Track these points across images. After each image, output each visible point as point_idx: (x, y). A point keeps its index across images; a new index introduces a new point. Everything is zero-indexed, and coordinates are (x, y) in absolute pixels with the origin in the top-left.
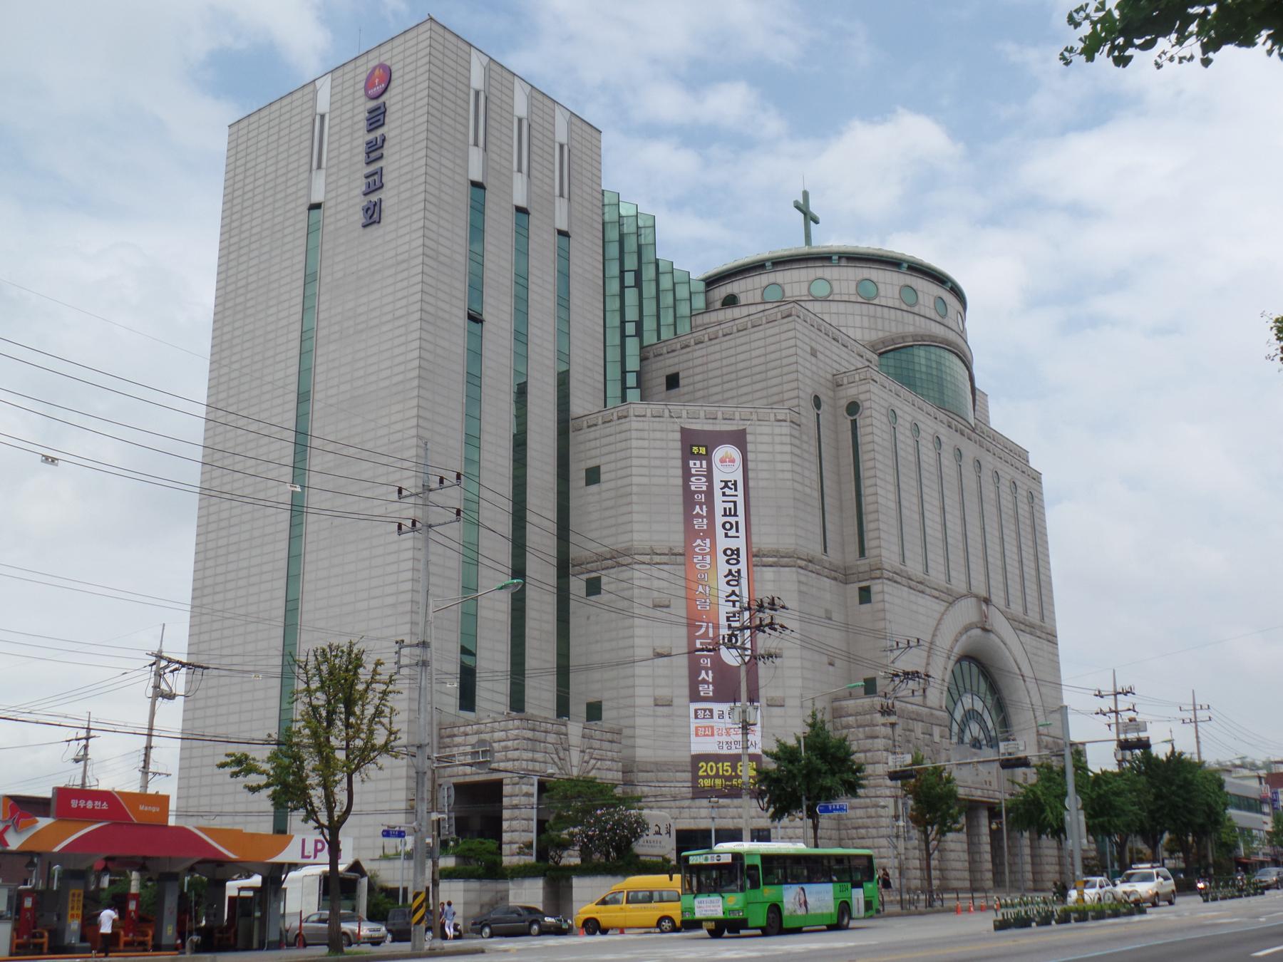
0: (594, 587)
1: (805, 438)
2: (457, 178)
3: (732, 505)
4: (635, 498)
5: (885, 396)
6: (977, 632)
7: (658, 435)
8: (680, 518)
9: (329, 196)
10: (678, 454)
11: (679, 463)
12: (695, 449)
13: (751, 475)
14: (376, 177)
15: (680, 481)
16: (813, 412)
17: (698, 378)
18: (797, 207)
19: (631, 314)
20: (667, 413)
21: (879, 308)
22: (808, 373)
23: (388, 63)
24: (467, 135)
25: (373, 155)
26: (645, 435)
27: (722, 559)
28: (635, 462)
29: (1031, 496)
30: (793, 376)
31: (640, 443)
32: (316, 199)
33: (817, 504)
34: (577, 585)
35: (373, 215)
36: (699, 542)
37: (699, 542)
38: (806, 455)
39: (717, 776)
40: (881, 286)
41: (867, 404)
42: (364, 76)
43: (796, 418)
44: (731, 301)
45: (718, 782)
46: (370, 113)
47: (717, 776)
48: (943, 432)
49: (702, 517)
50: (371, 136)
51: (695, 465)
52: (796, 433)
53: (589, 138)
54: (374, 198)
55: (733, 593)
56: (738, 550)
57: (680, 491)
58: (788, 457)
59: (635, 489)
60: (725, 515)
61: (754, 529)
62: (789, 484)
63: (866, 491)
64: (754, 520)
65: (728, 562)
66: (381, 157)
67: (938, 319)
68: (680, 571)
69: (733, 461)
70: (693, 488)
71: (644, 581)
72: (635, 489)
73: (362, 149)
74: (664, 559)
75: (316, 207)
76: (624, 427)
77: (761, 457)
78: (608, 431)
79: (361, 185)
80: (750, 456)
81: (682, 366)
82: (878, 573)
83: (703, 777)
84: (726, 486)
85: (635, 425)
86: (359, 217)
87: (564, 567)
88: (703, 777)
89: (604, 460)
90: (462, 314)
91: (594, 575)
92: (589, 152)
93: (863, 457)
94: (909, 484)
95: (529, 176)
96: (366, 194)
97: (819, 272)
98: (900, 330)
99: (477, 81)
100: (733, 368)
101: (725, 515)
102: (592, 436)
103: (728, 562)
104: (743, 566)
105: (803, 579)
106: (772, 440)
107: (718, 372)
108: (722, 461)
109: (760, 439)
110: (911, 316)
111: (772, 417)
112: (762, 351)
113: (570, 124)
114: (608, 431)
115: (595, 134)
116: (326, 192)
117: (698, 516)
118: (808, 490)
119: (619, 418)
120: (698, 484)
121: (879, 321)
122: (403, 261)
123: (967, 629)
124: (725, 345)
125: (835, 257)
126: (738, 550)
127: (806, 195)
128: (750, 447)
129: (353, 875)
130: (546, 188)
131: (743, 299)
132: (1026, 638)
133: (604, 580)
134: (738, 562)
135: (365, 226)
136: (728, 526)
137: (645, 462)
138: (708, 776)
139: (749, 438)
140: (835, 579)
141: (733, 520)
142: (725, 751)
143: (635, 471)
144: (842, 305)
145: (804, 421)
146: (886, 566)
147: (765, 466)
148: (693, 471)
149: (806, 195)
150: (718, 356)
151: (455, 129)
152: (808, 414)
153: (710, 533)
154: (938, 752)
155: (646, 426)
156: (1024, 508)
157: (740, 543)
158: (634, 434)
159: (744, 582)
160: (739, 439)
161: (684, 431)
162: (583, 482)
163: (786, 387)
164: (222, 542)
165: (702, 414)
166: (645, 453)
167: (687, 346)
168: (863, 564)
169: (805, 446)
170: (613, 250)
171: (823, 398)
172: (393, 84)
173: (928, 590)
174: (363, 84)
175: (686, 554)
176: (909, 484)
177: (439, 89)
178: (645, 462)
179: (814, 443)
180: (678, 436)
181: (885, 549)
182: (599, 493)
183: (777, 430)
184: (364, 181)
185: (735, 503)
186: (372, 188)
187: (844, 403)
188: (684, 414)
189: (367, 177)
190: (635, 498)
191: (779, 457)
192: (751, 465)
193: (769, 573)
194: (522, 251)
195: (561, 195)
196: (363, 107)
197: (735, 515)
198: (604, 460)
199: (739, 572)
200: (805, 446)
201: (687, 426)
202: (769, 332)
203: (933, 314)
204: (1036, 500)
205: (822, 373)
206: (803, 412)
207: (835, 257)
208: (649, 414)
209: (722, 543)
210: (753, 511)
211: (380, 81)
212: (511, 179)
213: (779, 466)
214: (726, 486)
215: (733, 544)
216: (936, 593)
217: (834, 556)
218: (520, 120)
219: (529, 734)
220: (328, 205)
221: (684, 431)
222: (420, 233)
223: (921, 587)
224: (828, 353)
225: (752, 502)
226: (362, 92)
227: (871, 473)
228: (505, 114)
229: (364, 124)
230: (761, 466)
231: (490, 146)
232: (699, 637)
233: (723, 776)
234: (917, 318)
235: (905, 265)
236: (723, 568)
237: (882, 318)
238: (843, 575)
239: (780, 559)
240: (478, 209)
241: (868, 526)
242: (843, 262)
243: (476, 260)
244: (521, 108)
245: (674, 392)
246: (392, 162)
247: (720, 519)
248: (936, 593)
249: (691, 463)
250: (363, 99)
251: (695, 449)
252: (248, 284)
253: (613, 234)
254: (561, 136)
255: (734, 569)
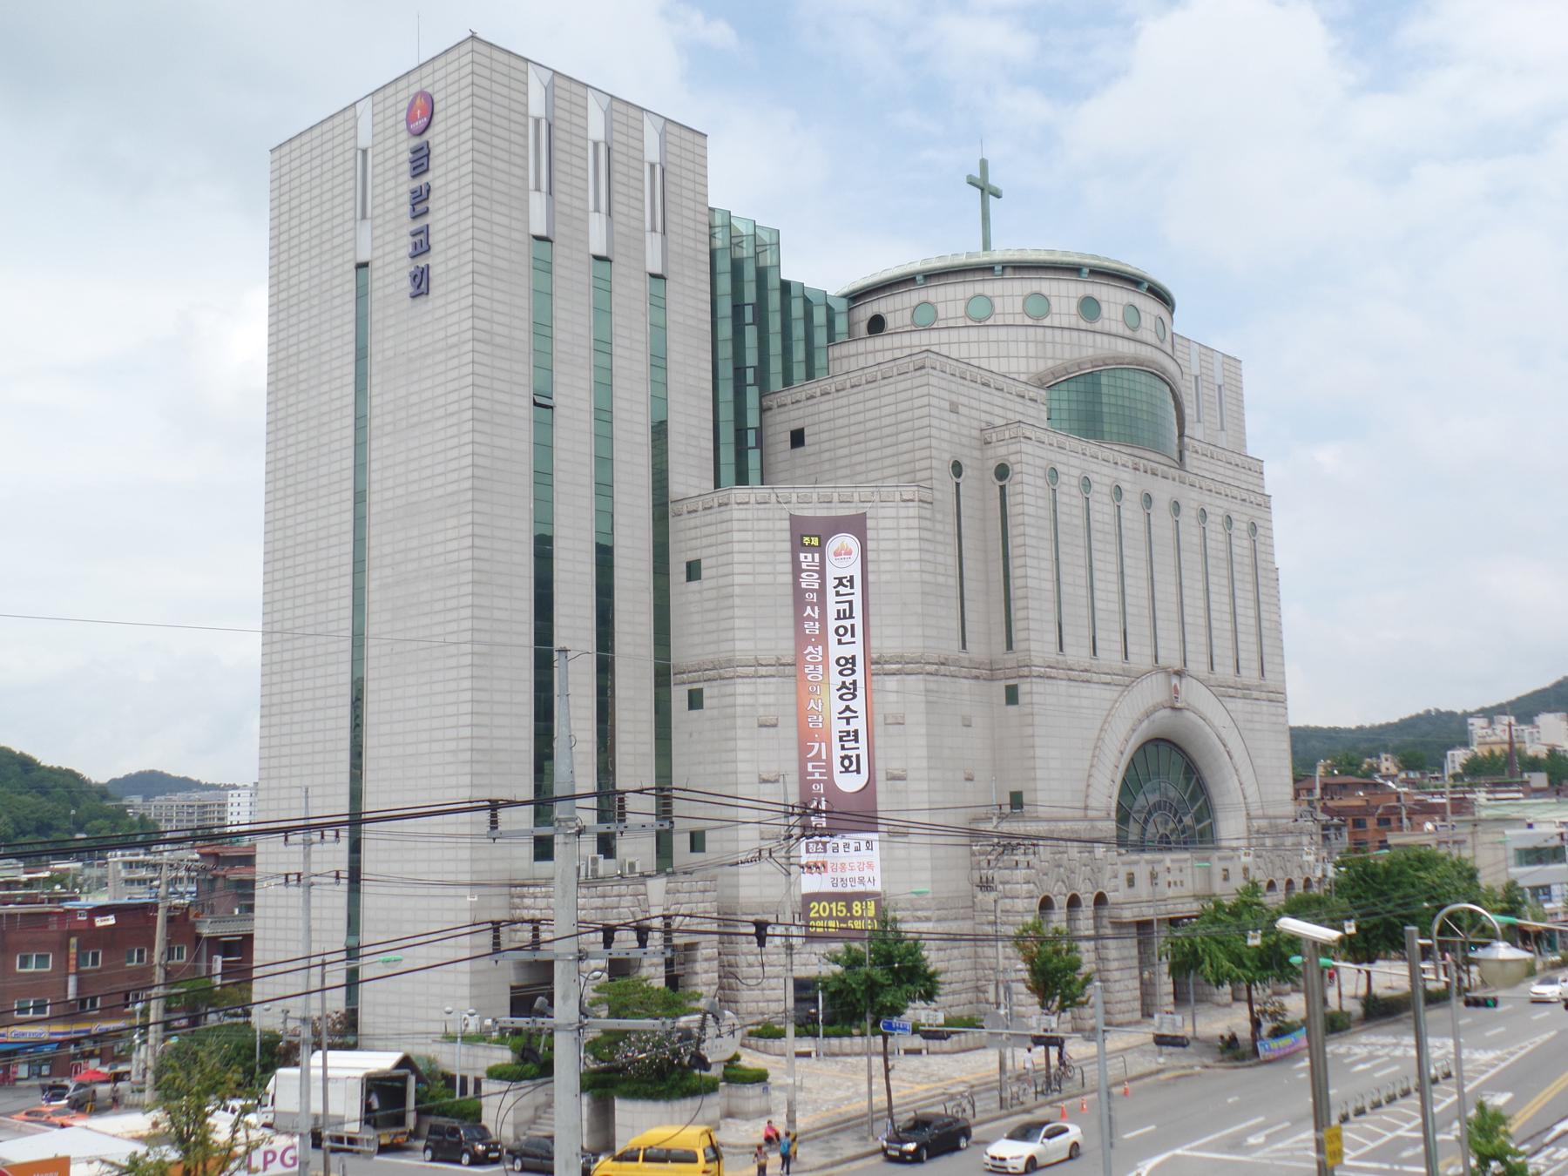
0: (695, 700)
1: (939, 516)
2: (516, 235)
3: (846, 606)
4: (737, 601)
5: (1043, 453)
6: (1167, 712)
7: (763, 525)
8: (791, 622)
9: (379, 252)
10: (788, 546)
11: (788, 557)
12: (806, 540)
13: (871, 567)
14: (422, 237)
15: (789, 579)
16: (951, 482)
17: (824, 436)
18: (972, 182)
19: (751, 358)
20: (773, 498)
21: (1049, 331)
22: (946, 435)
23: (429, 90)
24: (526, 179)
25: (419, 208)
26: (749, 525)
27: (834, 669)
28: (737, 557)
29: (1253, 528)
30: (926, 442)
31: (742, 536)
32: (362, 258)
33: (956, 592)
34: (679, 696)
35: (421, 283)
36: (810, 649)
37: (810, 649)
38: (940, 538)
39: (830, 917)
40: (1053, 301)
41: (1017, 468)
42: (405, 104)
43: (926, 495)
44: (877, 325)
45: (832, 924)
46: (414, 152)
47: (830, 917)
48: (1126, 478)
49: (813, 620)
50: (416, 184)
51: (806, 559)
52: (927, 514)
53: (689, 146)
54: (422, 262)
55: (847, 708)
56: (853, 658)
57: (789, 590)
58: (915, 544)
59: (737, 590)
60: (839, 618)
61: (873, 631)
62: (916, 576)
63: (1015, 572)
64: (873, 621)
65: (841, 673)
66: (426, 212)
67: (1128, 333)
68: (789, 686)
69: (849, 553)
70: (804, 585)
71: (750, 696)
72: (737, 590)
73: (406, 198)
74: (771, 670)
75: (362, 266)
76: (726, 516)
77: (883, 545)
78: (709, 519)
79: (406, 245)
80: (870, 545)
81: (808, 421)
82: (1025, 671)
83: (815, 919)
84: (841, 584)
85: (736, 514)
86: (406, 285)
87: (663, 677)
88: (815, 919)
89: (706, 552)
90: (527, 403)
91: (695, 686)
92: (691, 166)
93: (1012, 532)
94: (1073, 556)
95: (609, 214)
96: (413, 257)
97: (979, 288)
98: (1076, 355)
99: (537, 107)
100: (861, 427)
101: (839, 618)
102: (692, 523)
103: (841, 673)
104: (859, 676)
105: (933, 686)
106: (898, 526)
107: (845, 431)
108: (837, 554)
109: (882, 524)
110: (1090, 336)
111: (898, 497)
112: (892, 409)
113: (663, 135)
114: (709, 519)
115: (698, 139)
116: (373, 249)
117: (810, 618)
118: (941, 579)
119: (720, 505)
120: (809, 581)
121: (1049, 346)
122: (455, 346)
123: (1155, 709)
124: (853, 399)
125: (998, 268)
126: (853, 658)
127: (984, 164)
128: (870, 534)
129: (402, 1072)
130: (634, 223)
131: (891, 323)
132: (1237, 705)
133: (706, 693)
134: (854, 672)
135: (414, 296)
136: (841, 631)
137: (749, 557)
138: (820, 918)
139: (870, 523)
140: (977, 678)
141: (847, 623)
142: (840, 889)
143: (737, 569)
144: (1003, 331)
145: (938, 495)
146: (1036, 661)
147: (888, 556)
148: (804, 566)
149: (984, 164)
150: (845, 411)
151: (510, 174)
152: (944, 484)
153: (822, 639)
154: (1100, 870)
155: (749, 515)
156: (1241, 545)
157: (857, 650)
158: (736, 525)
159: (860, 692)
160: (856, 525)
161: (794, 519)
162: (684, 577)
163: (918, 455)
164: (287, 656)
165: (815, 497)
166: (748, 547)
167: (812, 397)
168: (1011, 659)
169: (939, 527)
170: (725, 284)
171: (964, 462)
172: (436, 119)
173: (1095, 677)
174: (403, 115)
175: (798, 662)
176: (1073, 556)
177: (486, 127)
178: (749, 557)
179: (953, 519)
180: (786, 525)
181: (1037, 642)
182: (700, 592)
183: (903, 513)
184: (411, 240)
185: (851, 603)
186: (420, 250)
187: (993, 464)
188: (794, 499)
189: (414, 234)
190: (737, 601)
191: (904, 545)
192: (871, 556)
193: (891, 683)
194: (602, 311)
195: (653, 230)
196: (404, 146)
197: (851, 617)
198: (706, 552)
199: (854, 683)
200: (939, 527)
201: (798, 513)
202: (901, 386)
203: (1119, 328)
204: (1260, 531)
205: (965, 431)
206: (936, 484)
207: (998, 268)
208: (753, 500)
209: (836, 651)
210: (872, 610)
211: (423, 113)
212: (586, 221)
213: (905, 555)
214: (841, 584)
215: (847, 651)
216: (1108, 678)
217: (976, 650)
218: (596, 144)
219: (598, 902)
220: (376, 264)
221: (794, 519)
222: (469, 313)
223: (1086, 676)
224: (974, 403)
225: (872, 600)
226: (403, 125)
227: (1020, 551)
228: (575, 140)
229: (407, 167)
230: (883, 556)
231: (557, 186)
232: (811, 760)
233: (837, 918)
234: (1098, 337)
235: (1086, 270)
236: (836, 680)
237: (1053, 342)
238: (989, 671)
239: (905, 666)
240: (544, 267)
241: (1017, 615)
242: (1008, 271)
243: (542, 329)
244: (596, 129)
245: (799, 450)
246: (440, 219)
247: (832, 624)
248: (1108, 678)
249: (802, 556)
250: (405, 135)
251: (806, 540)
252: (299, 353)
253: (724, 265)
254: (652, 153)
255: (848, 680)
